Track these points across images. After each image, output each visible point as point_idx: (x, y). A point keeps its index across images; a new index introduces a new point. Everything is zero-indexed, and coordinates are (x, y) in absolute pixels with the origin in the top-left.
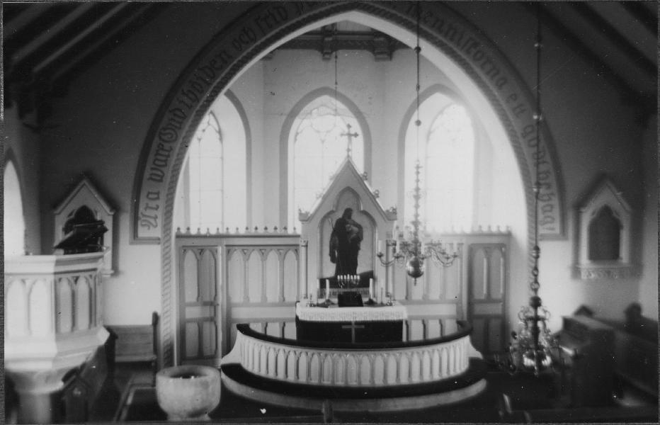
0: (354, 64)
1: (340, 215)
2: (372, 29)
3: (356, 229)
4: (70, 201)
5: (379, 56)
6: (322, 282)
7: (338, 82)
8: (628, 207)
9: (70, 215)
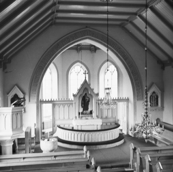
0: (85, 55)
1: (84, 94)
2: (91, 44)
3: (88, 99)
4: (12, 92)
5: (92, 52)
6: (79, 113)
7: (82, 59)
8: (160, 92)
9: (12, 96)
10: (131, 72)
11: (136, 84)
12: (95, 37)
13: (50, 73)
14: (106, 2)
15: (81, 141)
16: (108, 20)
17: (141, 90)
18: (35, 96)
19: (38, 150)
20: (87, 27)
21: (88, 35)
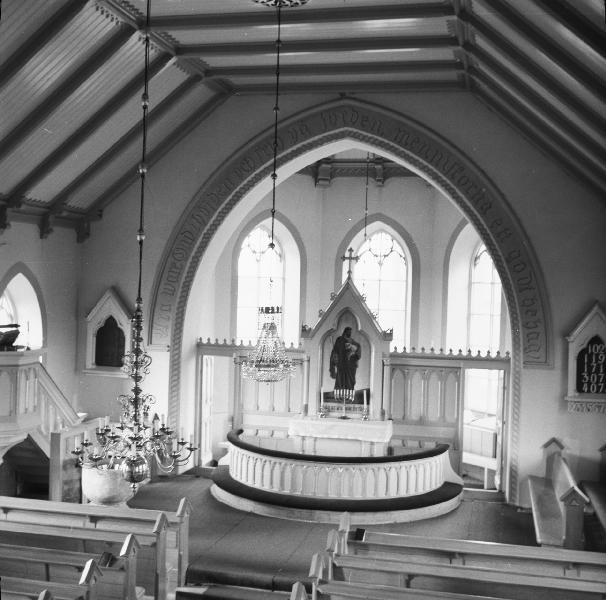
1: (341, 333)
3: (355, 348)
10: (503, 259)
11: (522, 305)
12: (371, 131)
13: (280, 256)
14: (274, 9)
15: (295, 490)
16: (278, 70)
17: (540, 329)
18: (167, 327)
19: (75, 495)
20: (343, 96)
21: (345, 124)
